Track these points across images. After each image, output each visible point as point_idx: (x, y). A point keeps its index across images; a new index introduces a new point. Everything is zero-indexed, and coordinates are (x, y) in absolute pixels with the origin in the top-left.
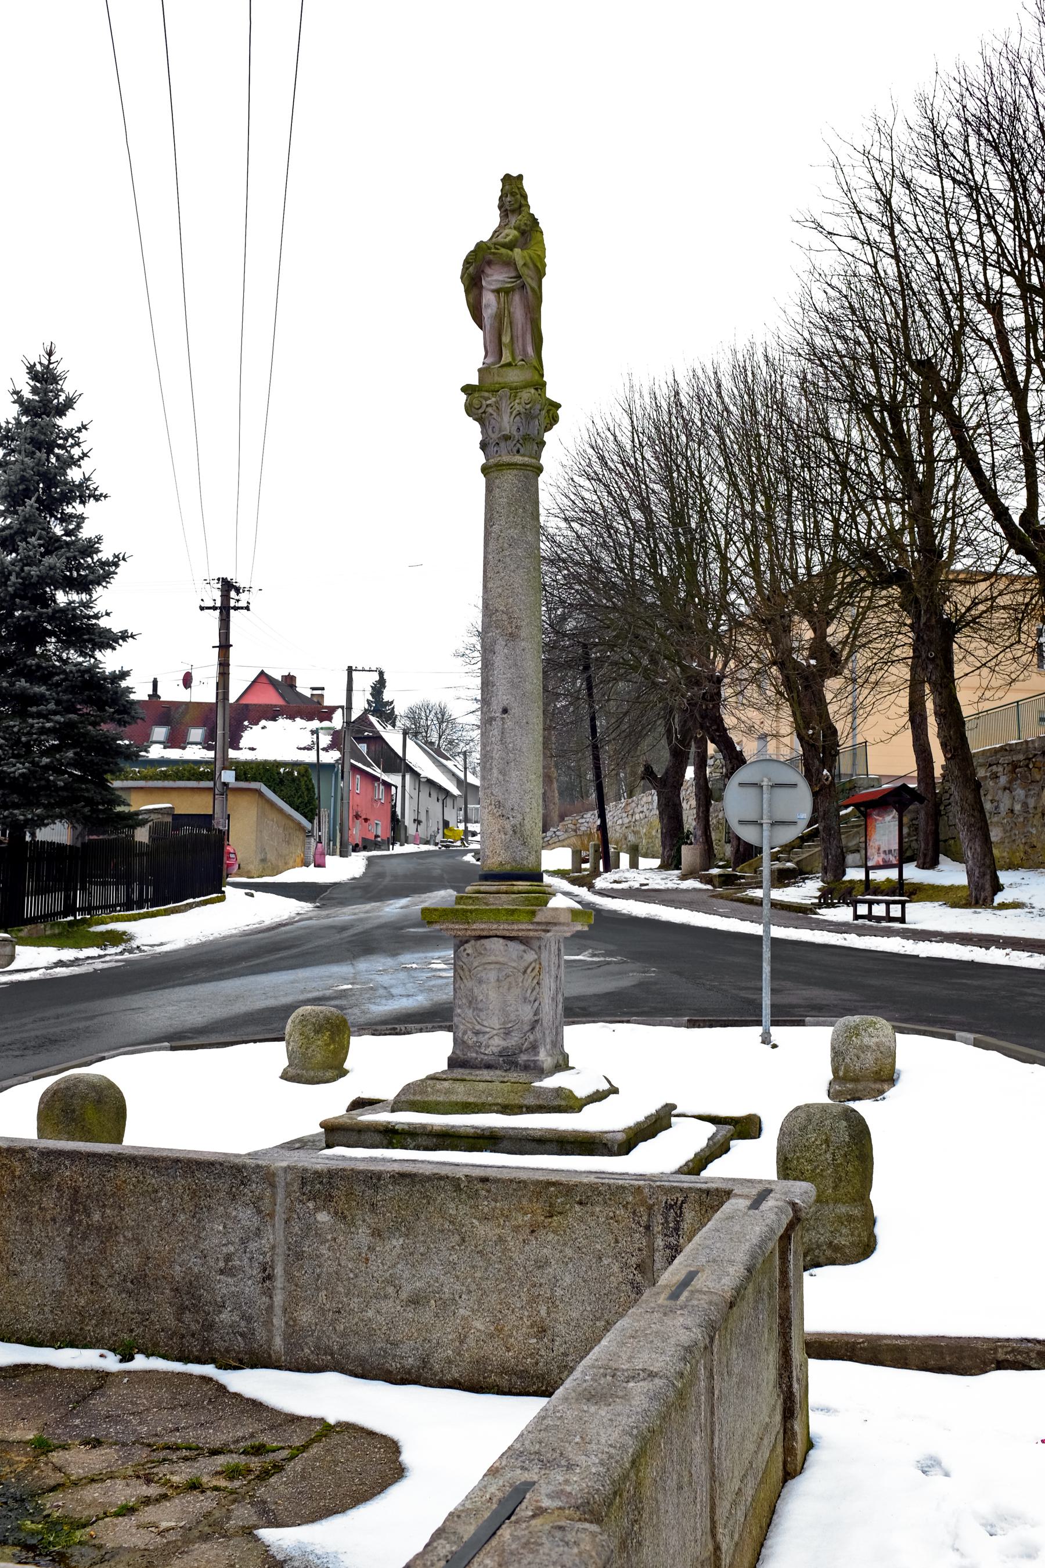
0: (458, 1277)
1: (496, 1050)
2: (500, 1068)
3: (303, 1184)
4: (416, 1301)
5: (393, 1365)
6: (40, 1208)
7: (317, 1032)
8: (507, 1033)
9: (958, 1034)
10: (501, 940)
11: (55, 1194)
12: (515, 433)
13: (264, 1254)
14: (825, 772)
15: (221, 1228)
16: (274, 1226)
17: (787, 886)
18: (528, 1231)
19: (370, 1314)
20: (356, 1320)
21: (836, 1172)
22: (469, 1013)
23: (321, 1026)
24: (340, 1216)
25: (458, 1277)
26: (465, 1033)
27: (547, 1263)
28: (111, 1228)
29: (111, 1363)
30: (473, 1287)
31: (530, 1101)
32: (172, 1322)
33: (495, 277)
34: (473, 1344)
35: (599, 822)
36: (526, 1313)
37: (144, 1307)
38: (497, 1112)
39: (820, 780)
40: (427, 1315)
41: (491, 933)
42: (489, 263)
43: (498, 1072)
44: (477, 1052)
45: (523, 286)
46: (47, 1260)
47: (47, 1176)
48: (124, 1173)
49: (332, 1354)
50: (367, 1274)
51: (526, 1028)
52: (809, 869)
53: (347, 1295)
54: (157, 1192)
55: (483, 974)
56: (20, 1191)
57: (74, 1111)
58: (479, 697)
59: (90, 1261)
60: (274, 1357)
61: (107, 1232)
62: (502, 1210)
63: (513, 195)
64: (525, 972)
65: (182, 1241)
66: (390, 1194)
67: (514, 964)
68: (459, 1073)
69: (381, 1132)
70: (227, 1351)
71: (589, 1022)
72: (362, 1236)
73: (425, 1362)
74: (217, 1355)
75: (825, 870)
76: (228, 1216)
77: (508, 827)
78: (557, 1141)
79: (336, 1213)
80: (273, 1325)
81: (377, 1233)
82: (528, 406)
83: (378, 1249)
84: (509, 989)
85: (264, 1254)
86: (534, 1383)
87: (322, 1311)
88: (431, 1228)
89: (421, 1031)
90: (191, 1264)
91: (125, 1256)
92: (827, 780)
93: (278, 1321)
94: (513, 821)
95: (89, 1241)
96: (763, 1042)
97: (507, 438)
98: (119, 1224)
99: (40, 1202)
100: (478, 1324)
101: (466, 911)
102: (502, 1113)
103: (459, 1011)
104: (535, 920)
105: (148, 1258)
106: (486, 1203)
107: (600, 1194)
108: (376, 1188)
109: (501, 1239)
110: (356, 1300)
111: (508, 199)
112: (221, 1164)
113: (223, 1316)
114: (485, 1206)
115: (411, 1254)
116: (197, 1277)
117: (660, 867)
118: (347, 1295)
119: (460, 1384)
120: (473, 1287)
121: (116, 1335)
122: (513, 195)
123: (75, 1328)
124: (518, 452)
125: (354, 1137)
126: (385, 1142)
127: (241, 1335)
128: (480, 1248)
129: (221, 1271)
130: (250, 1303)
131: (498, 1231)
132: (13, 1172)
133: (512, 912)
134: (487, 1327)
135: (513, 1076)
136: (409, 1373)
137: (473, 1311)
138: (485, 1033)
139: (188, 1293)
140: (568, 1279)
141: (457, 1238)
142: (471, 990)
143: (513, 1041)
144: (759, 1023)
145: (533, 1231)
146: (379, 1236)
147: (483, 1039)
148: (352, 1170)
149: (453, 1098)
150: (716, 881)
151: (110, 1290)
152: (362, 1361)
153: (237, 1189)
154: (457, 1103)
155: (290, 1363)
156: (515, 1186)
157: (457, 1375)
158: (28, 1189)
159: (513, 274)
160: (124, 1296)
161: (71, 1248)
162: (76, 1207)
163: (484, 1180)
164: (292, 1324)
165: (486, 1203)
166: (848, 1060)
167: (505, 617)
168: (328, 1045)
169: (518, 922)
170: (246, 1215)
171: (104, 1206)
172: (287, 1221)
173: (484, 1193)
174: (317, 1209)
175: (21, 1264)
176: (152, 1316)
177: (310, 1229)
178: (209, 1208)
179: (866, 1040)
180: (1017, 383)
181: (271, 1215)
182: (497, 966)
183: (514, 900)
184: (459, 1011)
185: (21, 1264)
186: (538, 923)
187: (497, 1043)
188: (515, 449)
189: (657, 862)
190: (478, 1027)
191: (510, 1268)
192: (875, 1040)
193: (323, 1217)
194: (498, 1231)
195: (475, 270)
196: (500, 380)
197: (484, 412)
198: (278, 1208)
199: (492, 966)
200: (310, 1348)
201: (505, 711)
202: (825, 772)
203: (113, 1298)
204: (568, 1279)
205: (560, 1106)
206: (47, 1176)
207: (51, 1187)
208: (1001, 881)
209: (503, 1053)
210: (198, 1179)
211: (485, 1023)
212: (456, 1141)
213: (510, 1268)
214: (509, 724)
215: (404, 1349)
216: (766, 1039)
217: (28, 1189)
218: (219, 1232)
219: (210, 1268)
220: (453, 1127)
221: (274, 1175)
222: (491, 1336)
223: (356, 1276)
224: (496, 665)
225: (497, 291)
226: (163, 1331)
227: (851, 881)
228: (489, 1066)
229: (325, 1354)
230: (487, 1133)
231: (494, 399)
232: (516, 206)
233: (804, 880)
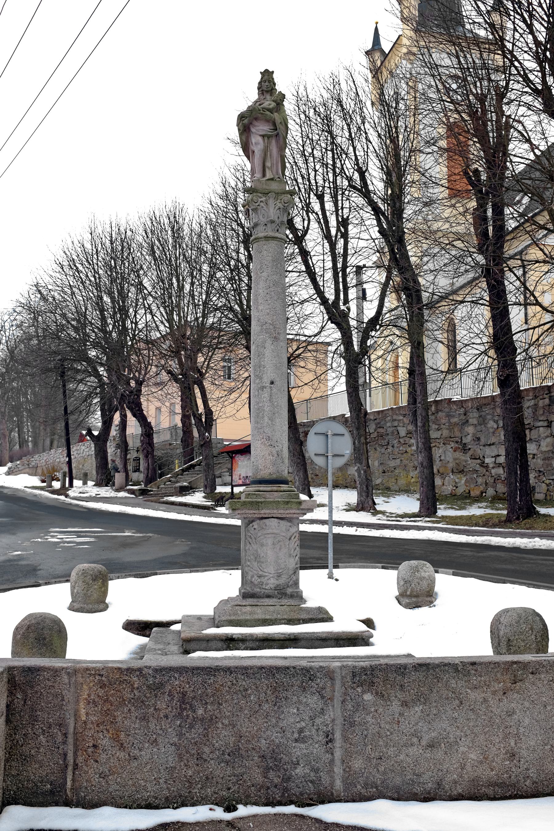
0: (458, 727)
1: (272, 586)
2: (276, 597)
3: (354, 676)
4: (431, 746)
5: (418, 789)
6: (155, 709)
7: (94, 580)
8: (279, 576)
9: (440, 570)
10: (276, 520)
11: (167, 698)
13: (327, 725)
14: (207, 434)
15: (295, 711)
16: (333, 706)
17: (185, 495)
18: (502, 693)
19: (402, 757)
20: (393, 762)
21: (538, 645)
22: (255, 564)
23: (96, 577)
24: (380, 695)
25: (458, 727)
26: (252, 577)
27: (514, 712)
28: (212, 719)
29: (219, 814)
30: (468, 732)
31: (304, 616)
32: (260, 779)
33: (261, 128)
34: (470, 769)
35: (67, 459)
36: (502, 746)
37: (238, 771)
38: (285, 624)
39: (204, 439)
40: (439, 754)
41: (270, 516)
42: (256, 119)
43: (274, 600)
44: (260, 588)
45: (277, 135)
46: (161, 746)
47: (161, 685)
48: (220, 679)
49: (376, 787)
50: (399, 731)
51: (291, 572)
52: (195, 486)
53: (386, 746)
54: (247, 690)
55: (264, 541)
56: (139, 698)
57: (44, 639)
59: (196, 743)
60: (335, 794)
61: (210, 722)
62: (485, 681)
63: (267, 82)
64: (290, 539)
65: (267, 722)
66: (414, 678)
67: (284, 534)
68: (250, 601)
69: (222, 640)
70: (302, 794)
71: (215, 570)
72: (395, 707)
73: (439, 784)
74: (294, 798)
75: (206, 487)
76: (300, 702)
78: (335, 639)
79: (377, 693)
80: (334, 772)
81: (405, 704)
82: (286, 205)
83: (406, 714)
84: (280, 549)
85: (327, 725)
86: (509, 790)
87: (369, 759)
88: (440, 697)
89: (118, 578)
90: (273, 737)
91: (223, 737)
93: (338, 770)
94: (277, 449)
95: (195, 729)
96: (329, 578)
97: (272, 222)
98: (218, 716)
99: (154, 705)
100: (472, 756)
101: (259, 502)
102: (287, 624)
103: (249, 563)
104: (301, 507)
106: (475, 678)
107: (544, 666)
108: (403, 674)
109: (485, 700)
110: (392, 749)
111: (267, 84)
112: (294, 668)
113: (297, 771)
114: (474, 680)
115: (428, 715)
116: (278, 746)
117: (94, 485)
118: (386, 746)
119: (463, 796)
120: (468, 732)
121: (217, 793)
122: (267, 82)
123: (185, 793)
125: (204, 644)
126: (225, 646)
127: (311, 782)
128: (472, 707)
129: (296, 740)
130: (318, 759)
131: (483, 695)
132: (132, 685)
133: (288, 503)
134: (478, 757)
135: (285, 601)
136: (429, 793)
137: (469, 747)
138: (265, 576)
139: (272, 758)
140: (527, 721)
141: (457, 702)
142: (257, 551)
144: (326, 567)
145: (504, 693)
146: (406, 705)
147: (264, 580)
148: (386, 664)
149: (256, 617)
150: (137, 493)
151: (212, 762)
152: (397, 789)
153: (307, 684)
154: (259, 620)
155: (348, 797)
156: (492, 666)
157: (460, 791)
158: (145, 696)
160: (223, 765)
161: (180, 735)
162: (184, 706)
163: (473, 664)
164: (348, 770)
165: (475, 678)
166: (413, 585)
167: (271, 327)
168: (101, 588)
169: (291, 508)
170: (313, 701)
171: (206, 703)
172: (343, 702)
173: (473, 672)
174: (364, 692)
175: (140, 750)
176: (245, 776)
177: (359, 706)
178: (286, 698)
179: (423, 574)
181: (332, 699)
182: (273, 535)
183: (282, 495)
184: (249, 563)
185: (140, 750)
186: (302, 509)
188: (276, 229)
189: (94, 483)
190: (261, 573)
191: (491, 718)
192: (427, 574)
193: (368, 697)
194: (483, 695)
195: (246, 122)
196: (267, 188)
198: (336, 693)
199: (270, 536)
200: (361, 785)
201: (272, 383)
202: (207, 434)
203: (215, 768)
204: (527, 721)
205: (323, 618)
206: (161, 685)
207: (164, 693)
208: (312, 493)
210: (278, 679)
211: (265, 570)
212: (271, 643)
213: (491, 718)
215: (425, 777)
216: (331, 576)
217: (145, 696)
219: (288, 739)
220: (269, 634)
221: (333, 672)
222: (481, 762)
223: (391, 734)
225: (263, 136)
226: (253, 786)
227: (220, 493)
228: (268, 596)
229: (372, 788)
230: (292, 637)
233: (194, 492)
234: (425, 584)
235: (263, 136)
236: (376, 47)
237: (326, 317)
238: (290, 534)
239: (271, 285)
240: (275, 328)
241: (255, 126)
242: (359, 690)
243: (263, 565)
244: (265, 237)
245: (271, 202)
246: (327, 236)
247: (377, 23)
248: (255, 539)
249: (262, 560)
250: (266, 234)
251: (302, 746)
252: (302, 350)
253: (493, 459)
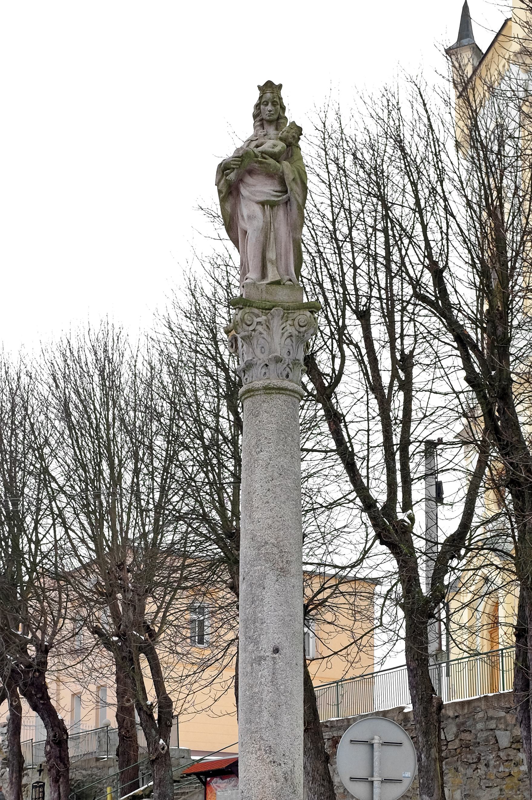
12: (285, 356)
14: (161, 741)
33: (259, 188)
39: (156, 749)
42: (251, 172)
45: (287, 202)
58: (515, 623)
77: (280, 774)
92: (163, 749)
97: (278, 360)
111: (269, 107)
124: (287, 376)
159: (278, 188)
180: (381, 388)
195: (233, 177)
196: (269, 298)
197: (254, 330)
201: (276, 650)
202: (161, 741)
214: (280, 664)
225: (263, 204)
231: (264, 317)
232: (275, 117)
235: (263, 204)
236: (465, 41)
237: (372, 533)
239: (276, 474)
240: (281, 551)
241: (249, 185)
246: (375, 387)
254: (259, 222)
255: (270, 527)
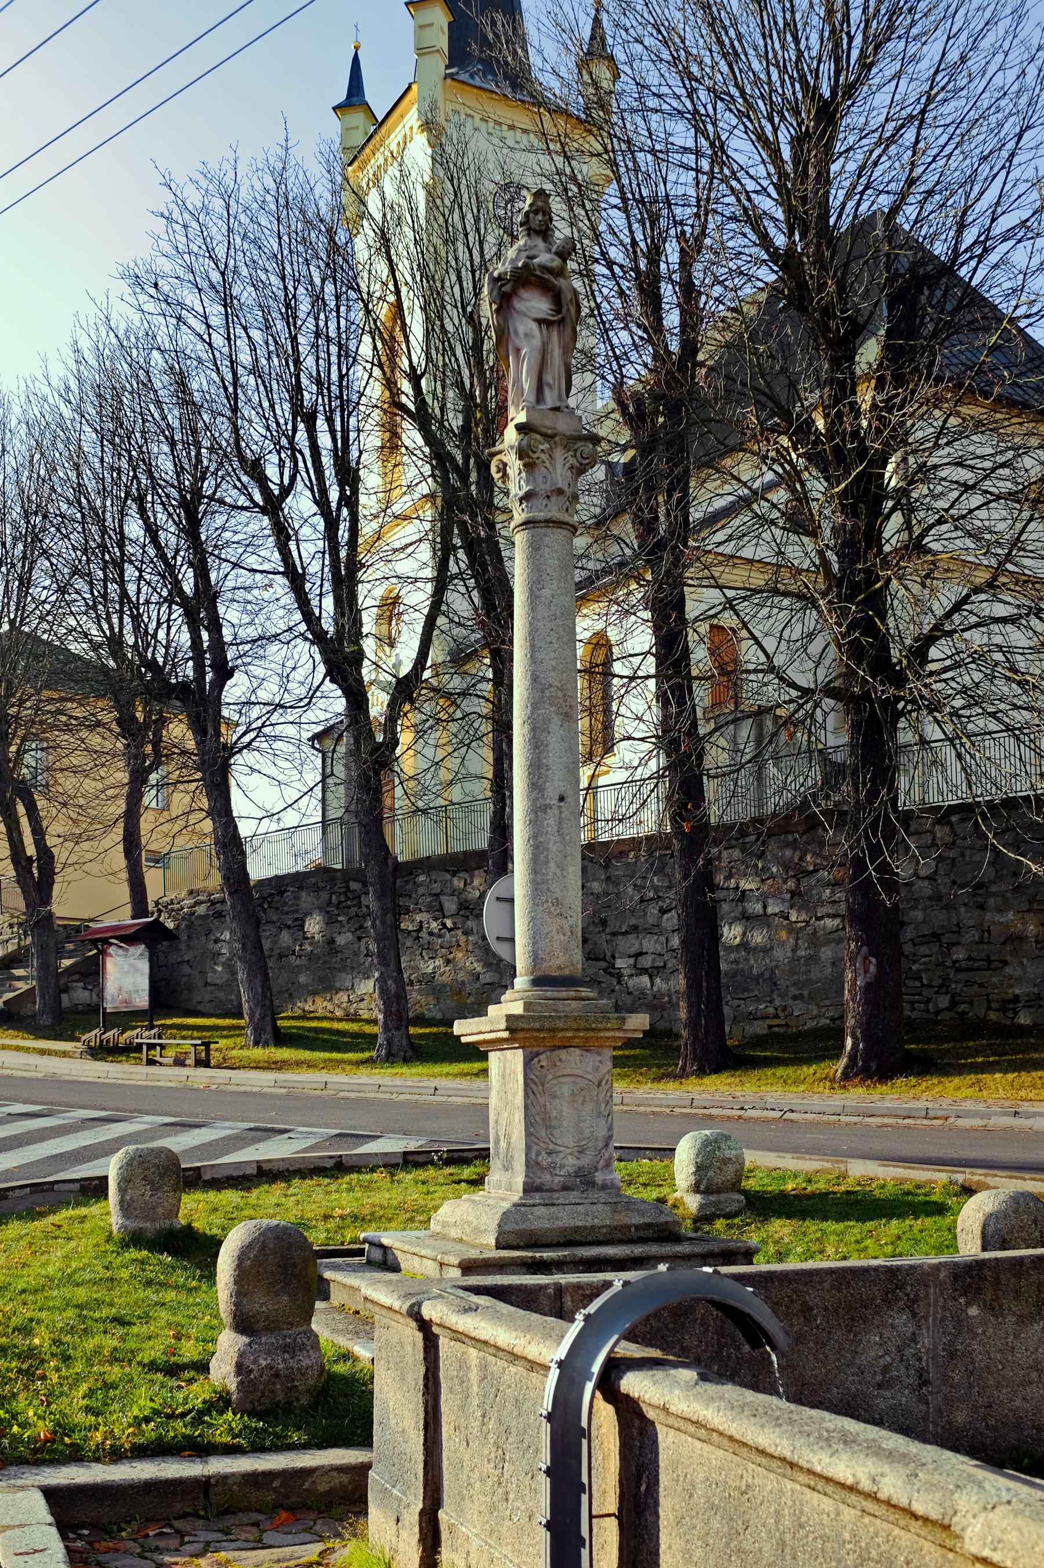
1: (571, 1170)
2: (578, 1188)
7: (162, 1176)
19: (1018, 1402)
26: (538, 1154)
51: (601, 1144)
57: (295, 1265)
64: (599, 1085)
68: (537, 1198)
77: (566, 927)
97: (560, 492)
105: (803, 1385)
111: (540, 217)
116: (854, 1396)
143: (586, 1161)
147: (558, 1159)
167: (560, 694)
170: (901, 1320)
174: (968, 1304)
182: (572, 1079)
187: (571, 1163)
190: (552, 1146)
193: (973, 1311)
199: (566, 1079)
201: (562, 799)
209: (579, 1173)
211: (559, 1142)
218: (876, 1343)
224: (551, 747)
225: (540, 322)
231: (547, 446)
234: (730, 1170)
235: (540, 322)
236: (354, 99)
237: (322, 669)
238: (598, 1076)
241: (522, 299)
242: (962, 1300)
243: (555, 1132)
244: (548, 521)
245: (559, 454)
247: (357, 48)
248: (543, 1085)
249: (554, 1123)
250: (549, 515)
251: (888, 1393)
252: (252, 735)
253: (632, 961)
254: (537, 342)
255: (554, 669)
